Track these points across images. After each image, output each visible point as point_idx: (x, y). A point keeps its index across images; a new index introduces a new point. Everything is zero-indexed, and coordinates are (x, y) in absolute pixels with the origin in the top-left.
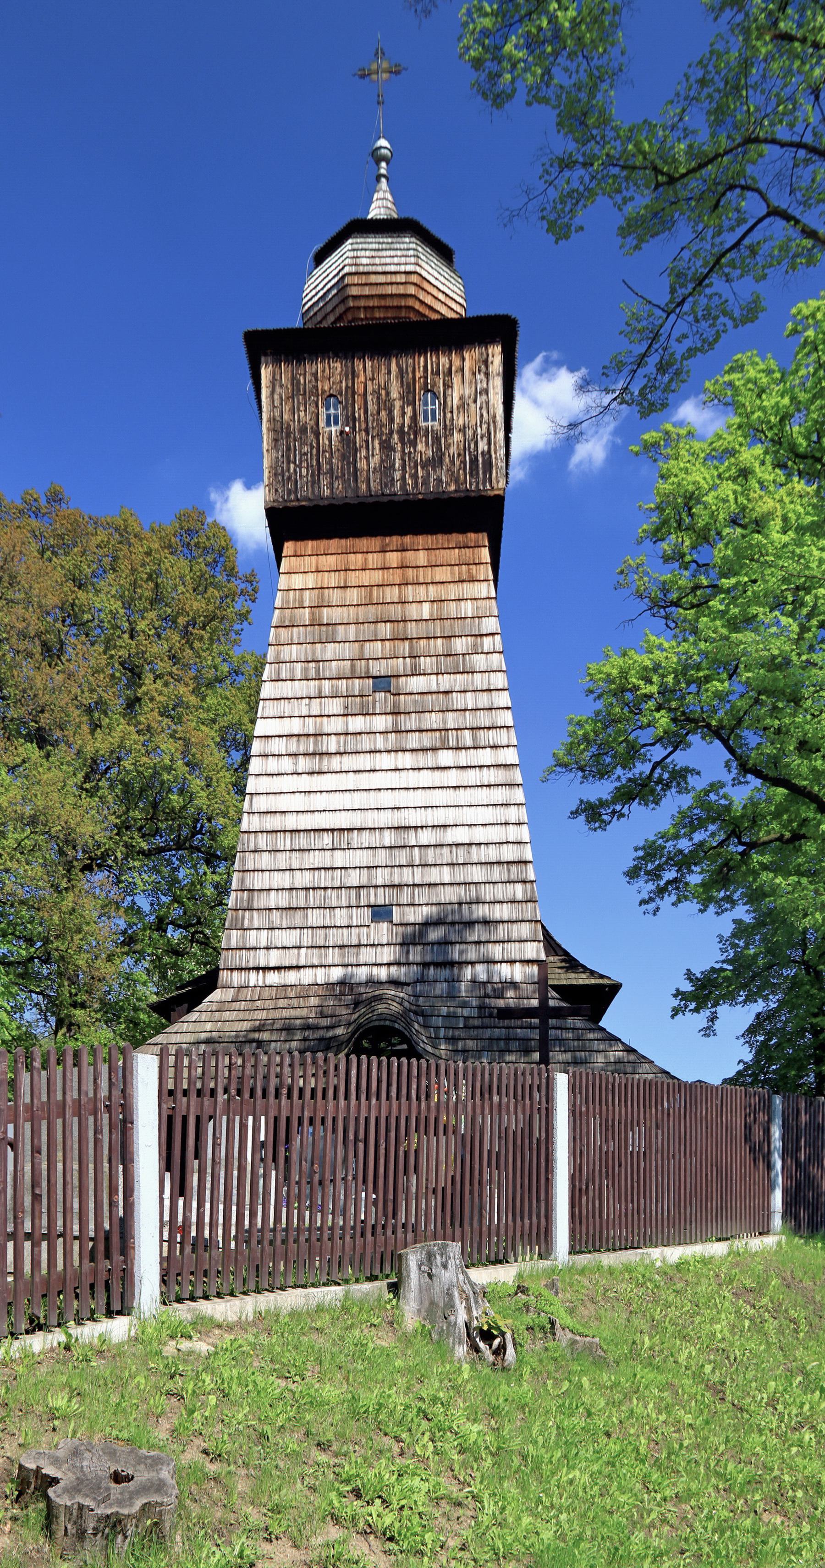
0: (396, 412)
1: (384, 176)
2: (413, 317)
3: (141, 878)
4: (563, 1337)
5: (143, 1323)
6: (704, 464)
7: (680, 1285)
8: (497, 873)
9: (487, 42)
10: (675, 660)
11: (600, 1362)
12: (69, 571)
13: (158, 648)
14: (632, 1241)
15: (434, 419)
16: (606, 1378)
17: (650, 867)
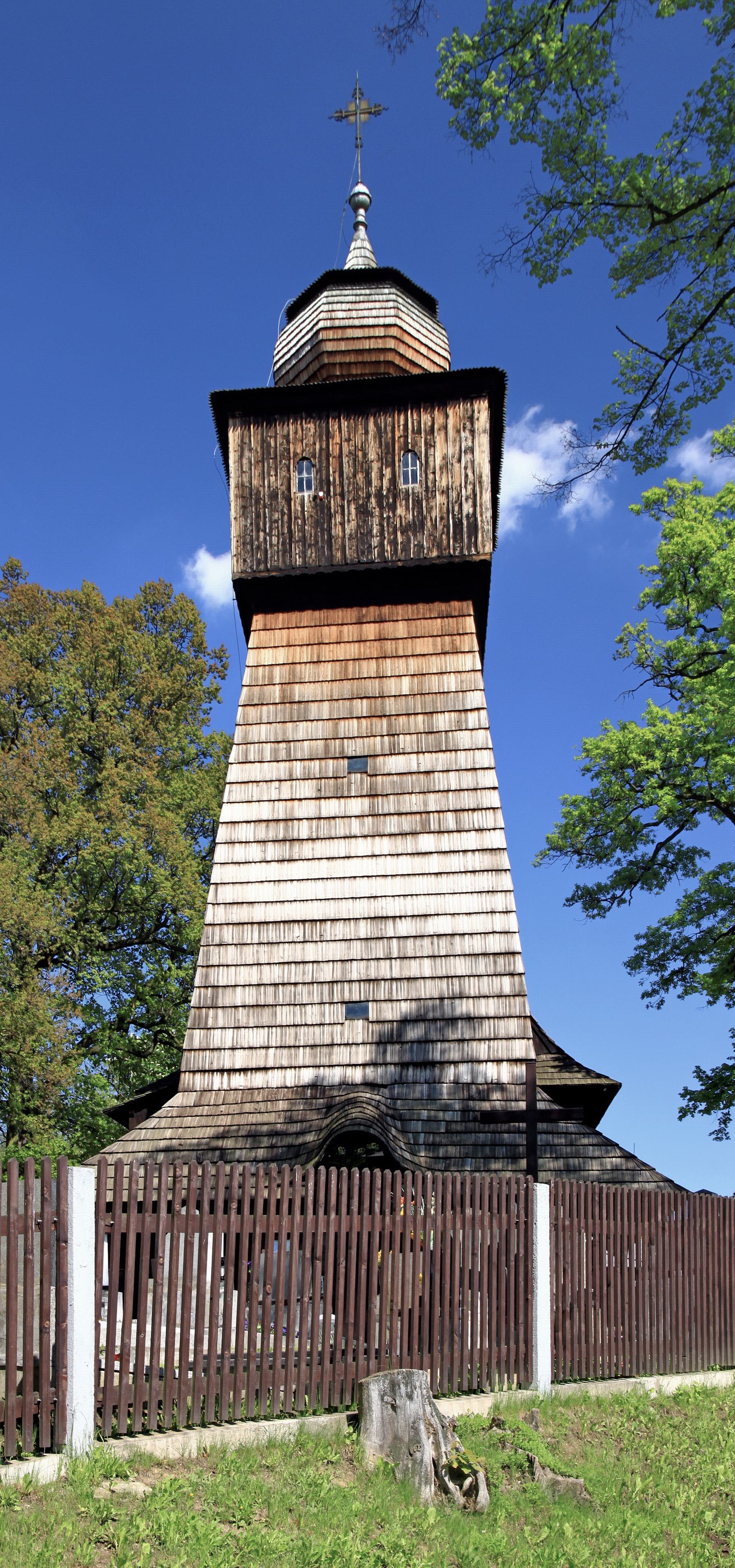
0: (374, 475)
1: (362, 223)
2: (393, 372)
3: (100, 973)
4: (544, 1477)
5: (74, 1460)
6: (710, 521)
7: (677, 1420)
8: (482, 965)
9: (467, 76)
10: (680, 733)
11: (585, 1507)
12: (26, 649)
13: (121, 730)
14: (624, 1369)
15: (414, 480)
16: (590, 1524)
17: (653, 956)
